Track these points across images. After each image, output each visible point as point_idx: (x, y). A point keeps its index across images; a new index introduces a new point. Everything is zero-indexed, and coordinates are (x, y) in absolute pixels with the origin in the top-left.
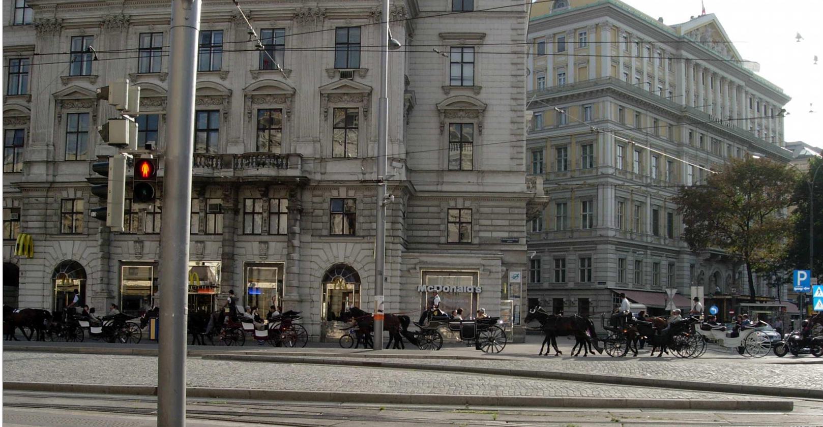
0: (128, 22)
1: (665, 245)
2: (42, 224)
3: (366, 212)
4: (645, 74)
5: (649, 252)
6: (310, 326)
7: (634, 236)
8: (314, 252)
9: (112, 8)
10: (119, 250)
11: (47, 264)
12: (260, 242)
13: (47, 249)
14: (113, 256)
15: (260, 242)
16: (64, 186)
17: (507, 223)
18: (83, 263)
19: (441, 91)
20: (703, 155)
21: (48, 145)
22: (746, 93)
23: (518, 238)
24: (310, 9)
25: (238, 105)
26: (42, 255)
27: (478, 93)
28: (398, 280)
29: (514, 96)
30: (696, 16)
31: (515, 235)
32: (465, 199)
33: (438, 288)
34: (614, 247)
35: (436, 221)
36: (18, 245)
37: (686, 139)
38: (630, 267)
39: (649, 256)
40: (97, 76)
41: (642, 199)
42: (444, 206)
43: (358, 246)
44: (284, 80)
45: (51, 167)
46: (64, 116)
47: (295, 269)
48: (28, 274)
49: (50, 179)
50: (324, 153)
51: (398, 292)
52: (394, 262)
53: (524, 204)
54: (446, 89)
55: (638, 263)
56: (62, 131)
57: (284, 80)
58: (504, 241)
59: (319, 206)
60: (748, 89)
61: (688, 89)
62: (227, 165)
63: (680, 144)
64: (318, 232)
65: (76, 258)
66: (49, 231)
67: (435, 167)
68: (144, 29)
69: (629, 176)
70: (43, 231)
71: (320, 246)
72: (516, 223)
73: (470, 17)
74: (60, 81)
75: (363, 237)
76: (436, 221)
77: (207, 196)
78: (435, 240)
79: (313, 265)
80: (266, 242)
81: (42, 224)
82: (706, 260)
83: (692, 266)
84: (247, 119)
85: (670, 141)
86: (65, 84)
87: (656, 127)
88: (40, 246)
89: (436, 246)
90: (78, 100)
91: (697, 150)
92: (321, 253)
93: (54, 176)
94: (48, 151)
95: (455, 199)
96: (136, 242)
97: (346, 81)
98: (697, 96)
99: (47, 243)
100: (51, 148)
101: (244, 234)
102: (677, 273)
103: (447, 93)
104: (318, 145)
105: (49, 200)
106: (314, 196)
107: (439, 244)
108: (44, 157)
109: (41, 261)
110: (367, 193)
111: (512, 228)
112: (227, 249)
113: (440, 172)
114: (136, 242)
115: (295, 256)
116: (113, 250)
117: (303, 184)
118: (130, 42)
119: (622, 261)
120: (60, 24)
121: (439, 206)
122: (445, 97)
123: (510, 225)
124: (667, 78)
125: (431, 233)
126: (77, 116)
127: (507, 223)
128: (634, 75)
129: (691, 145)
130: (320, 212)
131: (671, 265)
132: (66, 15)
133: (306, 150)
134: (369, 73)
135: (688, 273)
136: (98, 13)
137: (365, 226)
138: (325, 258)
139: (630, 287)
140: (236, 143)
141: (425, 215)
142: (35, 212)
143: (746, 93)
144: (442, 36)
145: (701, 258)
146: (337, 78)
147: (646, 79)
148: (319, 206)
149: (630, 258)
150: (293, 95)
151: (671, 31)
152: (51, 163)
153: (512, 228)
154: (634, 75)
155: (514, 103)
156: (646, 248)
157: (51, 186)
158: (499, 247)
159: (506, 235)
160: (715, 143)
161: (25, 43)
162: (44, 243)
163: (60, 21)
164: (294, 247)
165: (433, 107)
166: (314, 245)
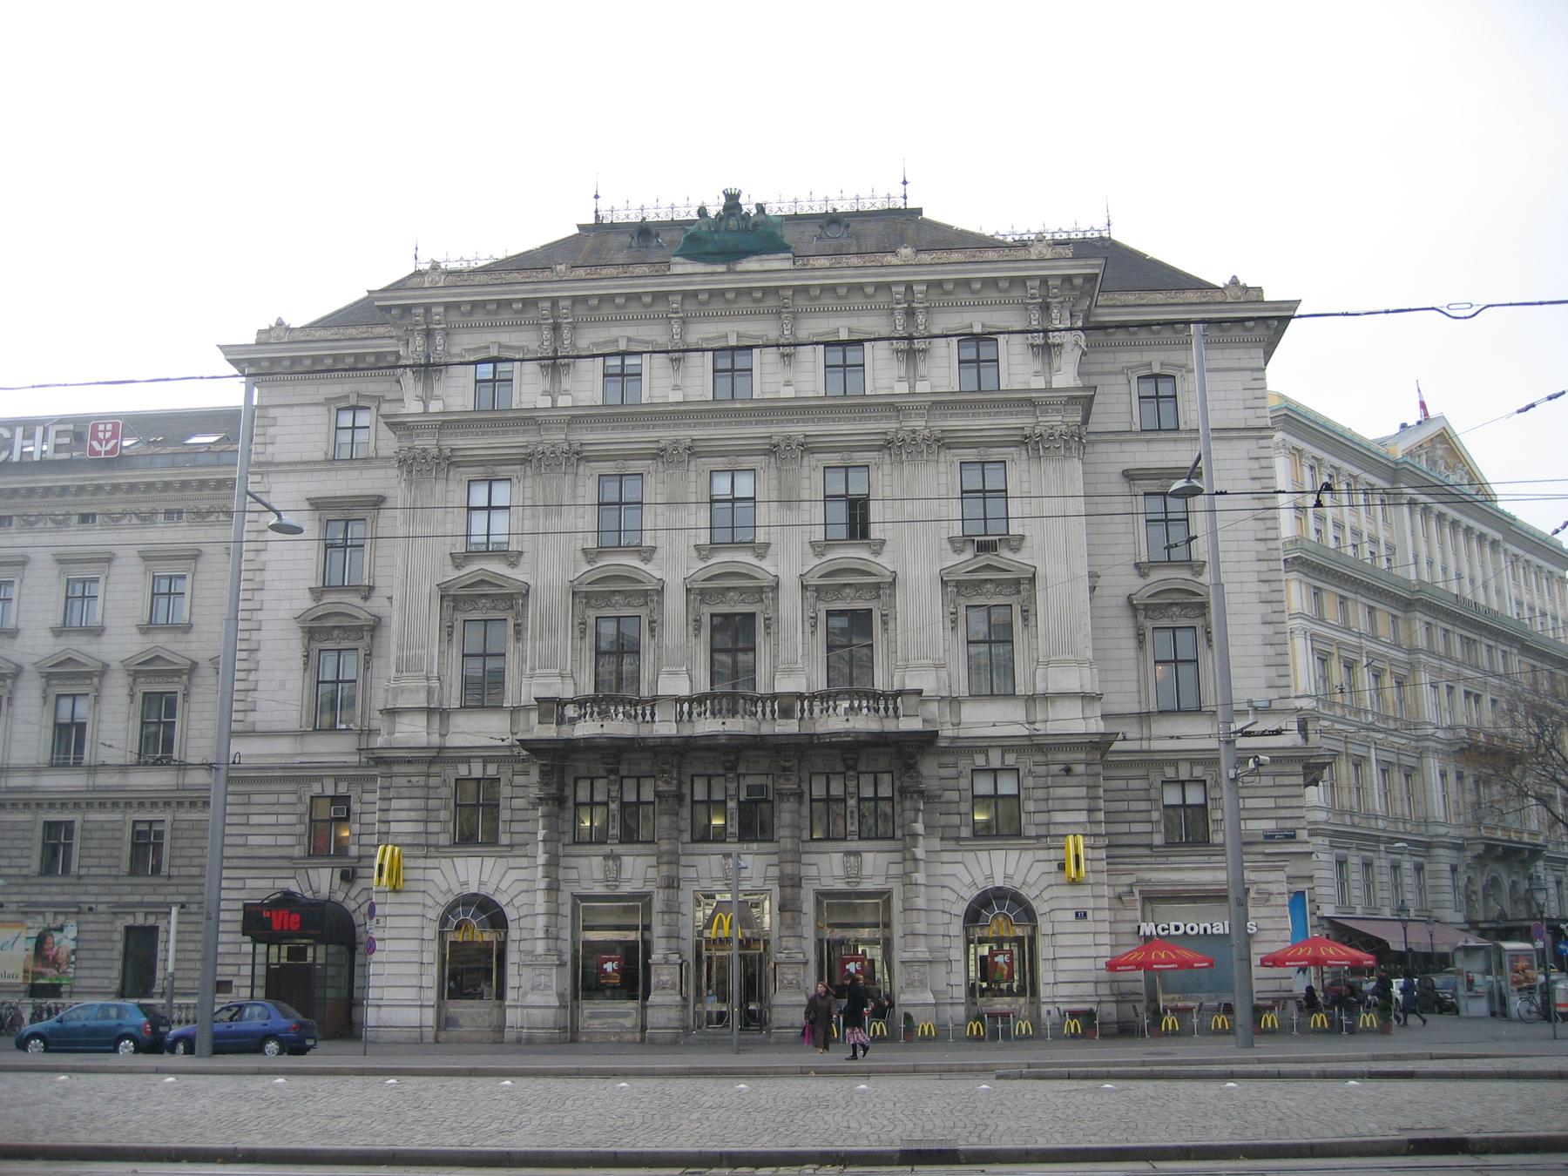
0: (579, 456)
1: (1353, 825)
2: (420, 827)
3: (1040, 793)
4: (1347, 528)
5: (1382, 847)
6: (948, 1008)
7: (1357, 820)
8: (946, 869)
9: (546, 430)
10: (573, 874)
11: (429, 902)
12: (848, 853)
13: (430, 874)
14: (563, 886)
15: (848, 853)
16: (464, 755)
17: (1270, 803)
18: (501, 899)
19: (1134, 571)
20: (1450, 667)
21: (428, 679)
22: (1506, 551)
23: (1294, 830)
24: (914, 432)
25: (791, 605)
26: (421, 886)
27: (1200, 574)
28: (1106, 915)
29: (1263, 577)
30: (1411, 422)
31: (1289, 824)
32: (1193, 762)
33: (1177, 928)
34: (1327, 841)
35: (1143, 806)
36: (381, 867)
37: (1421, 641)
38: (1355, 876)
39: (1383, 854)
40: (521, 553)
41: (1361, 751)
42: (965, 764)
43: (1028, 856)
44: (872, 558)
45: (436, 720)
46: (458, 625)
47: (920, 902)
48: (390, 922)
49: (435, 740)
50: (954, 687)
51: (1106, 939)
52: (1097, 884)
53: (1299, 769)
54: (1141, 569)
55: (1367, 865)
56: (456, 652)
57: (872, 558)
58: (1269, 837)
59: (951, 783)
60: (1508, 546)
61: (1416, 549)
62: (787, 713)
63: (1412, 650)
64: (954, 833)
65: (487, 890)
66: (433, 840)
67: (1135, 708)
68: (607, 467)
69: (1339, 712)
70: (422, 840)
71: (957, 856)
72: (1288, 802)
73: (1175, 440)
74: (449, 561)
75: (1038, 837)
76: (1143, 806)
77: (742, 770)
78: (1145, 840)
79: (946, 894)
80: (857, 853)
81: (420, 827)
82: (1479, 857)
83: (1454, 869)
84: (808, 629)
85: (1397, 646)
86: (458, 567)
87: (1345, 612)
88: (416, 869)
89: (1146, 851)
90: (486, 596)
91: (1440, 658)
92: (959, 870)
93: (442, 735)
94: (429, 690)
95: (1175, 763)
96: (606, 857)
97: (985, 559)
98: (1430, 563)
99: (430, 862)
100: (435, 684)
101: (812, 840)
102: (1429, 882)
103: (1143, 575)
104: (943, 674)
105: (433, 781)
106: (942, 766)
107: (1150, 846)
108: (420, 700)
109: (418, 897)
110: (1040, 758)
111: (1283, 813)
112: (789, 869)
113: (1143, 717)
114: (606, 857)
115: (920, 877)
116: (562, 874)
117: (926, 741)
118: (581, 491)
119: (1341, 863)
120: (448, 458)
121: (1146, 777)
122: (1142, 582)
123: (1277, 808)
124: (1382, 535)
125: (1136, 828)
126: (481, 626)
127: (1270, 803)
128: (1330, 531)
129: (1430, 652)
130: (955, 796)
131: (1419, 868)
132: (460, 443)
133: (927, 682)
134: (1027, 543)
135: (1449, 882)
136: (521, 439)
137: (1040, 818)
138: (967, 879)
139: (1359, 912)
140: (790, 671)
141: (1122, 795)
142: (406, 803)
143: (1506, 551)
144: (1129, 476)
145: (1469, 854)
146: (968, 554)
147: (1349, 538)
148: (951, 783)
149: (1354, 860)
150: (893, 583)
151: (1375, 447)
152: (436, 713)
153: (1283, 813)
154: (1330, 531)
155: (1265, 588)
156: (1377, 839)
157: (438, 757)
158: (1259, 848)
159: (1270, 825)
160: (1467, 642)
161: (357, 492)
162: (421, 863)
163: (447, 452)
164: (916, 860)
165: (1123, 601)
166: (946, 857)
